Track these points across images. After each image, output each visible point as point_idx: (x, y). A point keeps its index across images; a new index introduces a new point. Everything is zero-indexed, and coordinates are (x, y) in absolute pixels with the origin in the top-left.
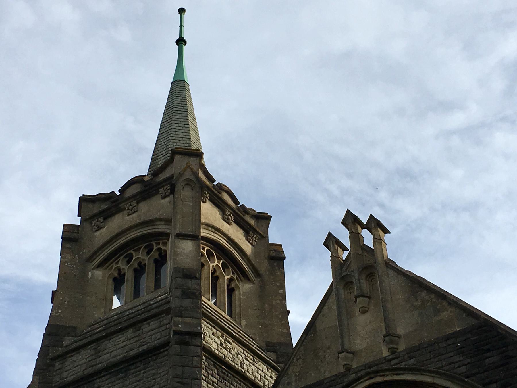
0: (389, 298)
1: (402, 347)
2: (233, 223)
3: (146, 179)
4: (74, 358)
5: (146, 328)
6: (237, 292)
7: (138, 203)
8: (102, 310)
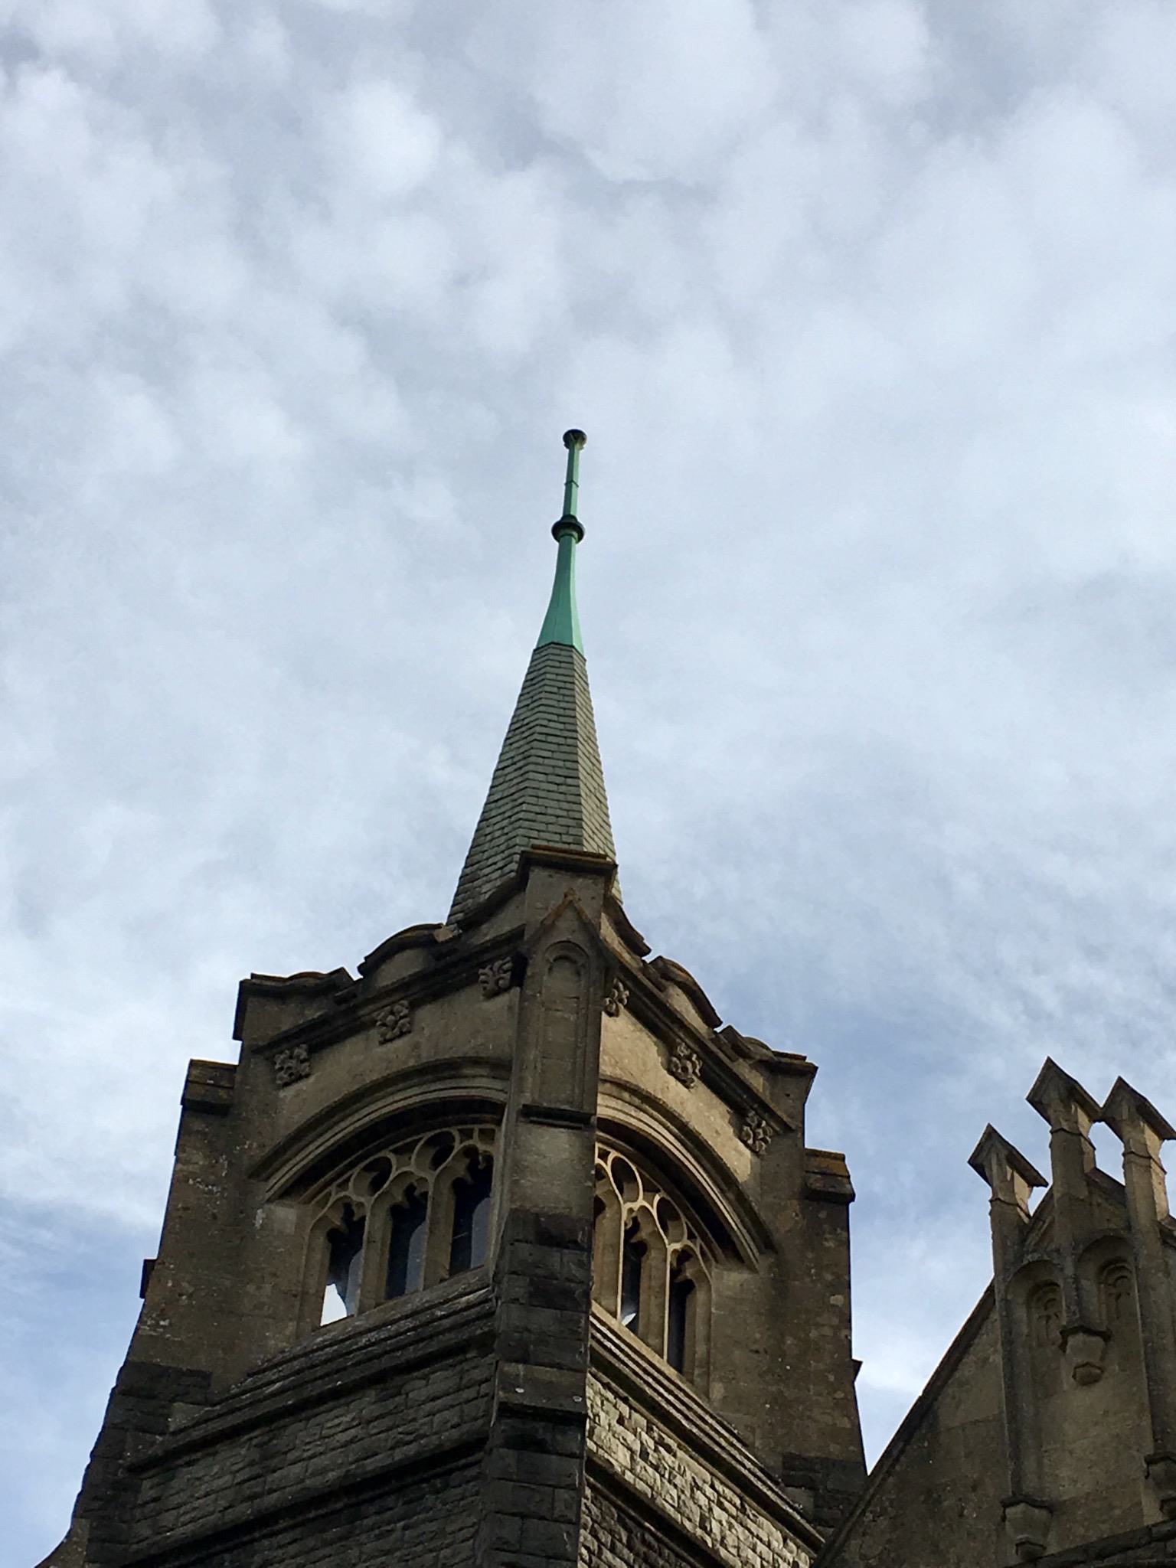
4: (197, 1470)
6: (700, 1296)
7: (414, 1006)
8: (291, 1327)
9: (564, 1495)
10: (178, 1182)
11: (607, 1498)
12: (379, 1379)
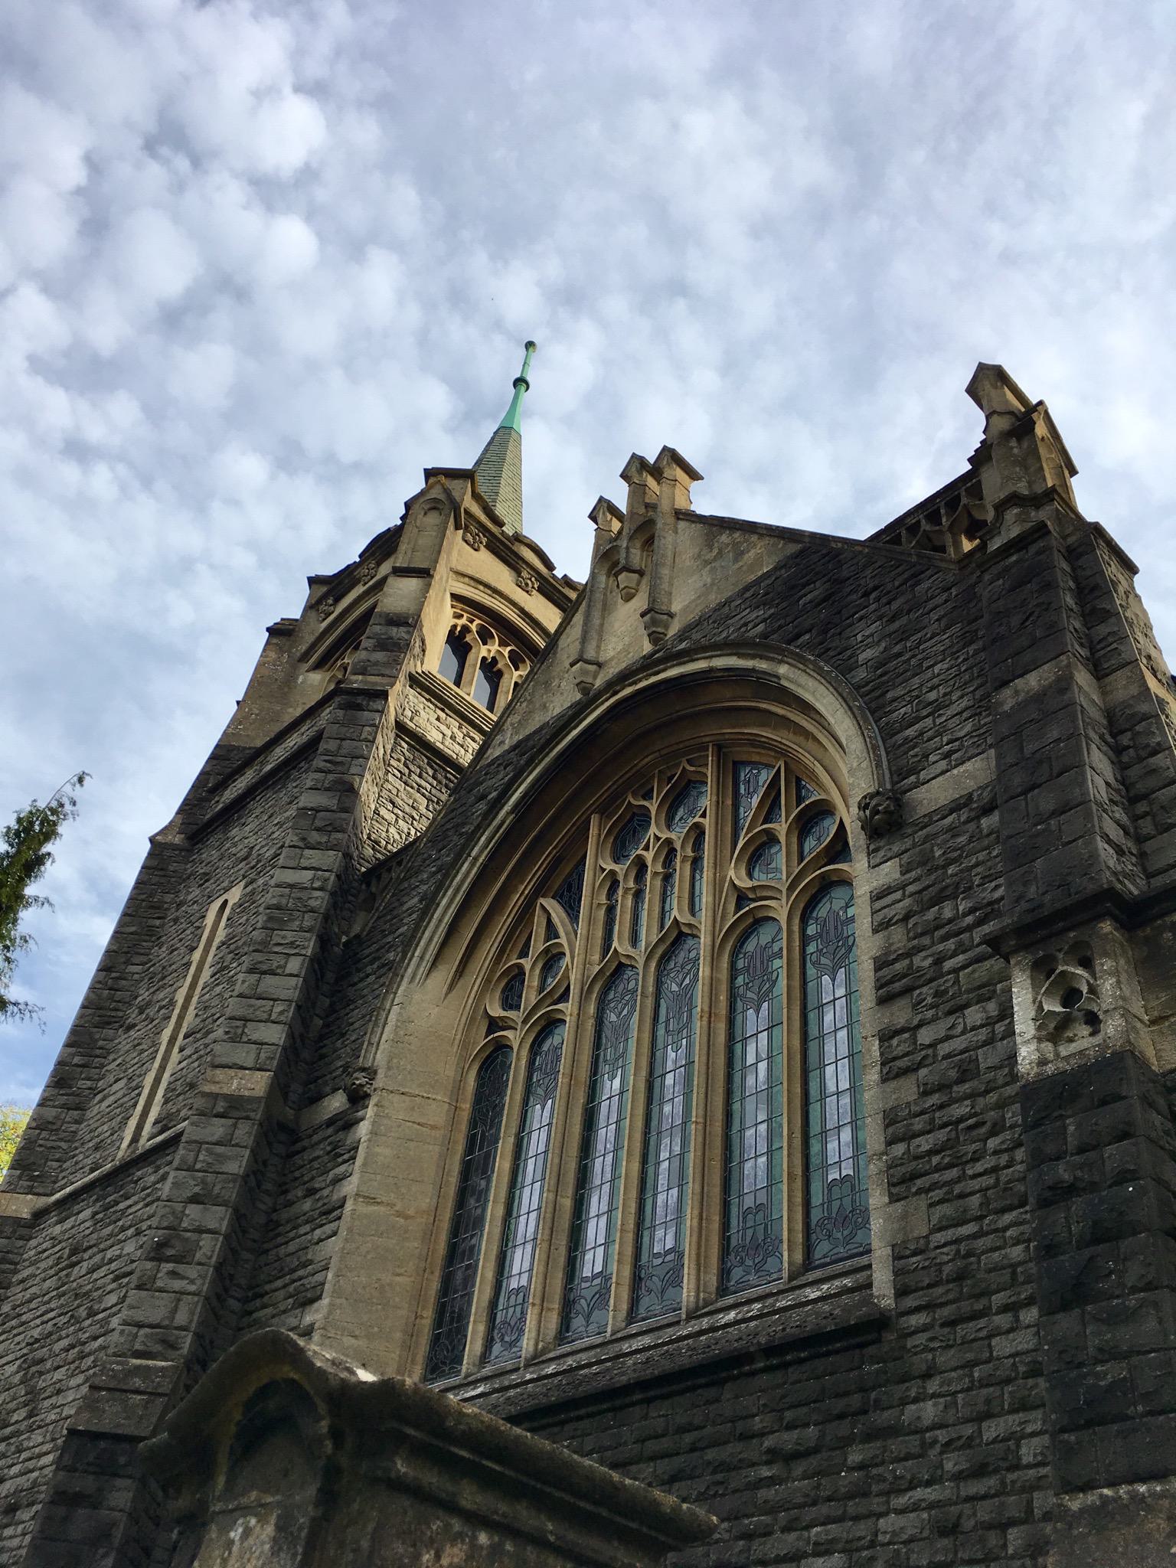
1: (674, 629)
9: (367, 729)
10: (260, 666)
11: (418, 750)
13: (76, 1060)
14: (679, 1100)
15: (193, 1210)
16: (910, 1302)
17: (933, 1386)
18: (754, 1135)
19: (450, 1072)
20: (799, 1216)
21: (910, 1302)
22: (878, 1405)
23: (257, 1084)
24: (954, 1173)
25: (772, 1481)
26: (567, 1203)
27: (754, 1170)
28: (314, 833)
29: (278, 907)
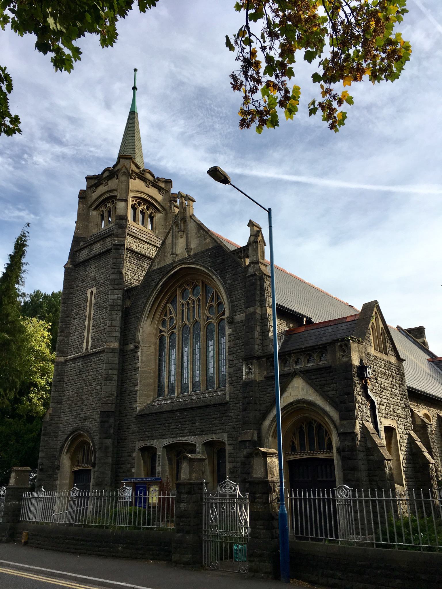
0: (190, 233)
1: (192, 253)
2: (151, 187)
3: (111, 169)
4: (83, 252)
5: (107, 240)
6: (155, 218)
7: (108, 181)
8: (96, 230)
9: (122, 255)
10: (79, 209)
12: (102, 239)
13: (63, 326)
14: (198, 355)
15: (110, 371)
16: (231, 400)
17: (233, 411)
18: (211, 365)
19: (153, 341)
20: (218, 379)
21: (231, 400)
22: (227, 413)
23: (115, 345)
24: (237, 384)
25: (214, 421)
26: (180, 370)
27: (211, 371)
28: (115, 285)
29: (111, 305)
